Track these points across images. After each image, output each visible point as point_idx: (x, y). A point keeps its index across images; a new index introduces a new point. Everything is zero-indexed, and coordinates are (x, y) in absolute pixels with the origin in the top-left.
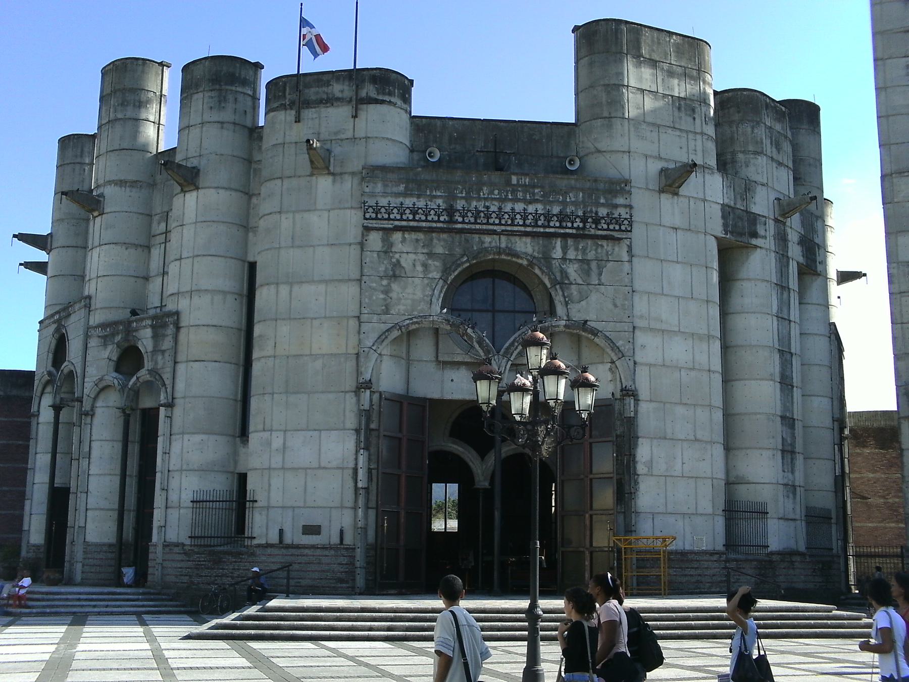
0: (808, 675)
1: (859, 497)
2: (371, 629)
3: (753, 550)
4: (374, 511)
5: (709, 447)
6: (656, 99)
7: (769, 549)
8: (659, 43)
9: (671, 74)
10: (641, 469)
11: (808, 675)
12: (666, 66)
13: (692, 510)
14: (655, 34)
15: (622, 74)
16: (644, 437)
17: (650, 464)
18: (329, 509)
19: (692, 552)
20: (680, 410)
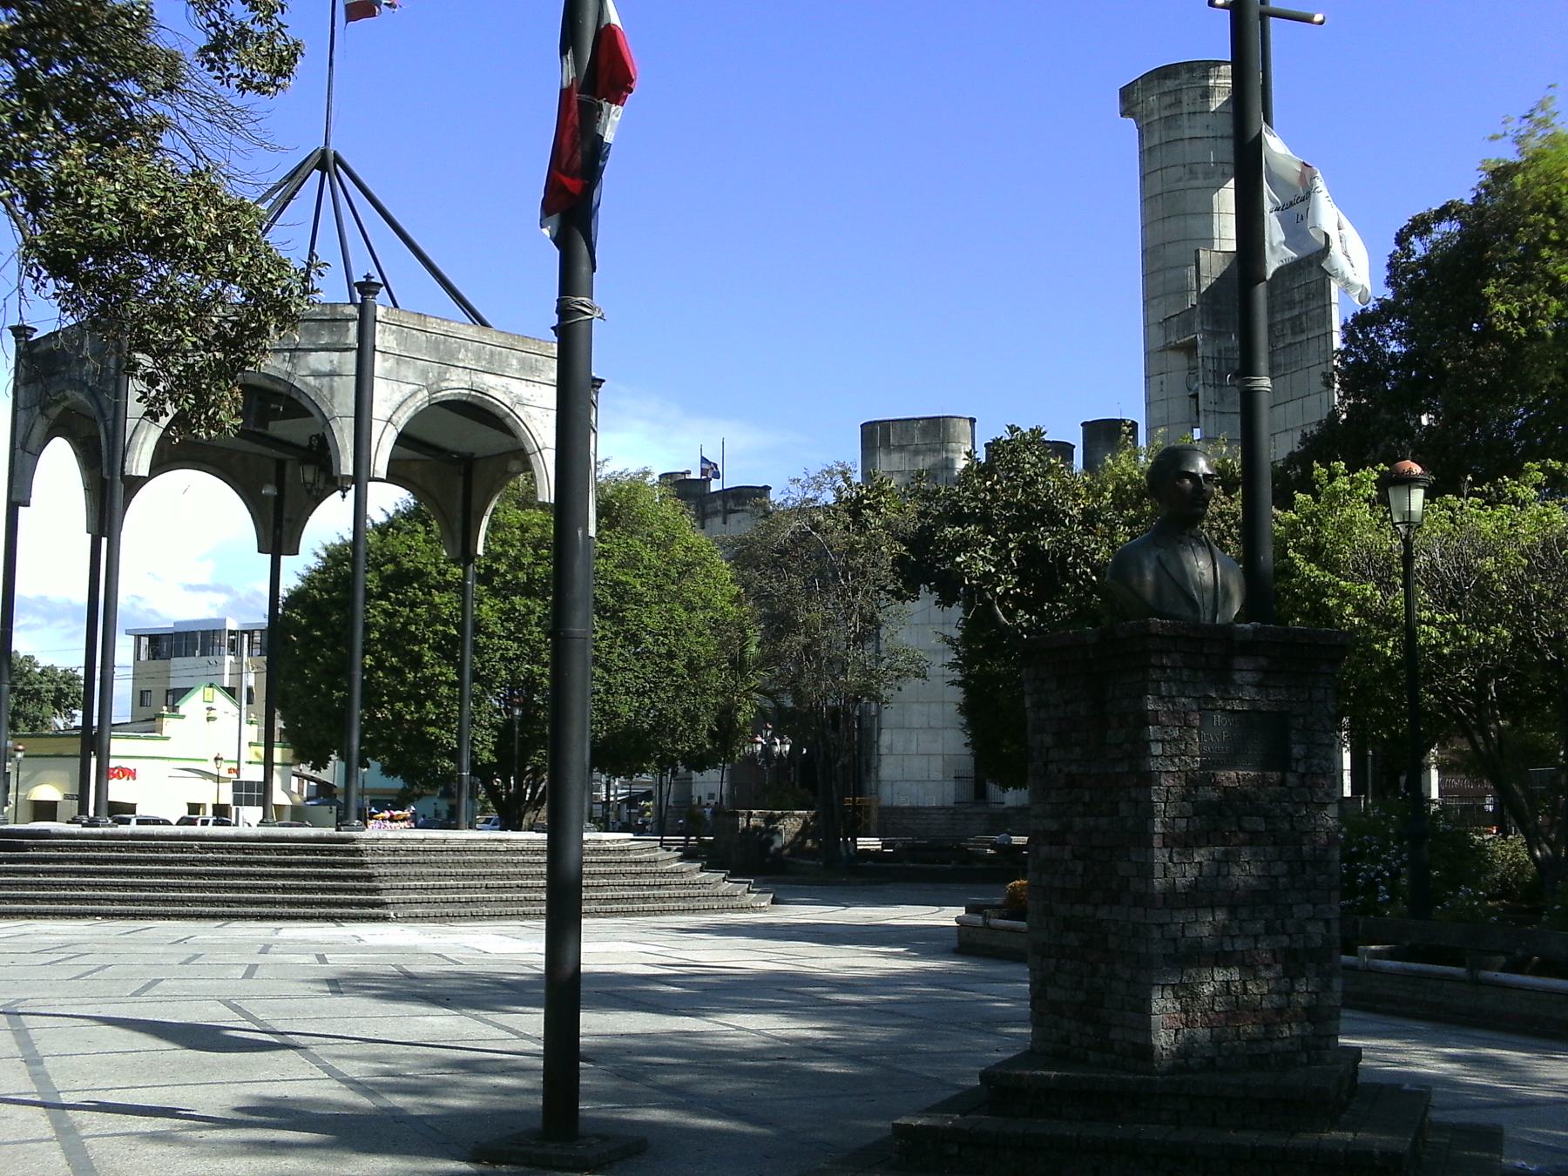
0: (26, 1094)
1: (111, 433)
2: (217, 888)
3: (996, 806)
4: (275, 761)
5: (941, 732)
6: (903, 476)
7: (1005, 806)
8: (907, 431)
9: (917, 453)
10: (883, 750)
11: (26, 1094)
12: (912, 448)
13: (926, 778)
14: (904, 424)
15: (875, 463)
16: (887, 728)
17: (891, 747)
18: (236, 759)
19: (921, 808)
20: (916, 707)
